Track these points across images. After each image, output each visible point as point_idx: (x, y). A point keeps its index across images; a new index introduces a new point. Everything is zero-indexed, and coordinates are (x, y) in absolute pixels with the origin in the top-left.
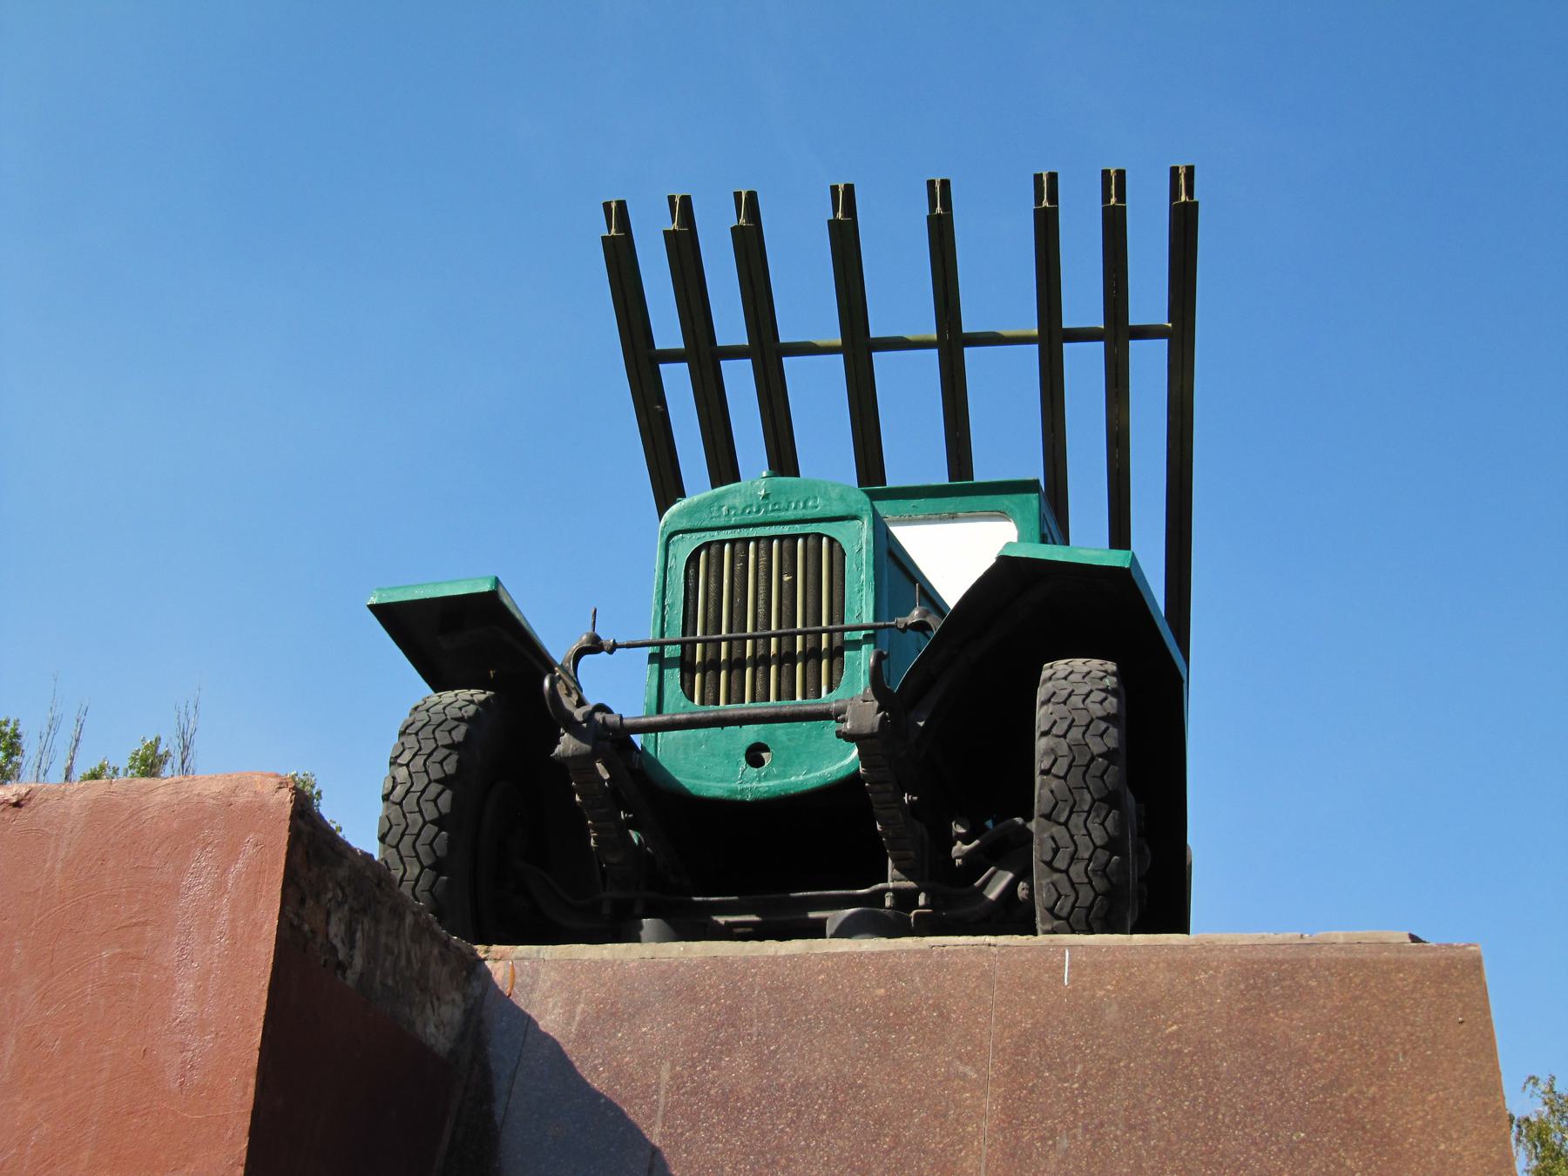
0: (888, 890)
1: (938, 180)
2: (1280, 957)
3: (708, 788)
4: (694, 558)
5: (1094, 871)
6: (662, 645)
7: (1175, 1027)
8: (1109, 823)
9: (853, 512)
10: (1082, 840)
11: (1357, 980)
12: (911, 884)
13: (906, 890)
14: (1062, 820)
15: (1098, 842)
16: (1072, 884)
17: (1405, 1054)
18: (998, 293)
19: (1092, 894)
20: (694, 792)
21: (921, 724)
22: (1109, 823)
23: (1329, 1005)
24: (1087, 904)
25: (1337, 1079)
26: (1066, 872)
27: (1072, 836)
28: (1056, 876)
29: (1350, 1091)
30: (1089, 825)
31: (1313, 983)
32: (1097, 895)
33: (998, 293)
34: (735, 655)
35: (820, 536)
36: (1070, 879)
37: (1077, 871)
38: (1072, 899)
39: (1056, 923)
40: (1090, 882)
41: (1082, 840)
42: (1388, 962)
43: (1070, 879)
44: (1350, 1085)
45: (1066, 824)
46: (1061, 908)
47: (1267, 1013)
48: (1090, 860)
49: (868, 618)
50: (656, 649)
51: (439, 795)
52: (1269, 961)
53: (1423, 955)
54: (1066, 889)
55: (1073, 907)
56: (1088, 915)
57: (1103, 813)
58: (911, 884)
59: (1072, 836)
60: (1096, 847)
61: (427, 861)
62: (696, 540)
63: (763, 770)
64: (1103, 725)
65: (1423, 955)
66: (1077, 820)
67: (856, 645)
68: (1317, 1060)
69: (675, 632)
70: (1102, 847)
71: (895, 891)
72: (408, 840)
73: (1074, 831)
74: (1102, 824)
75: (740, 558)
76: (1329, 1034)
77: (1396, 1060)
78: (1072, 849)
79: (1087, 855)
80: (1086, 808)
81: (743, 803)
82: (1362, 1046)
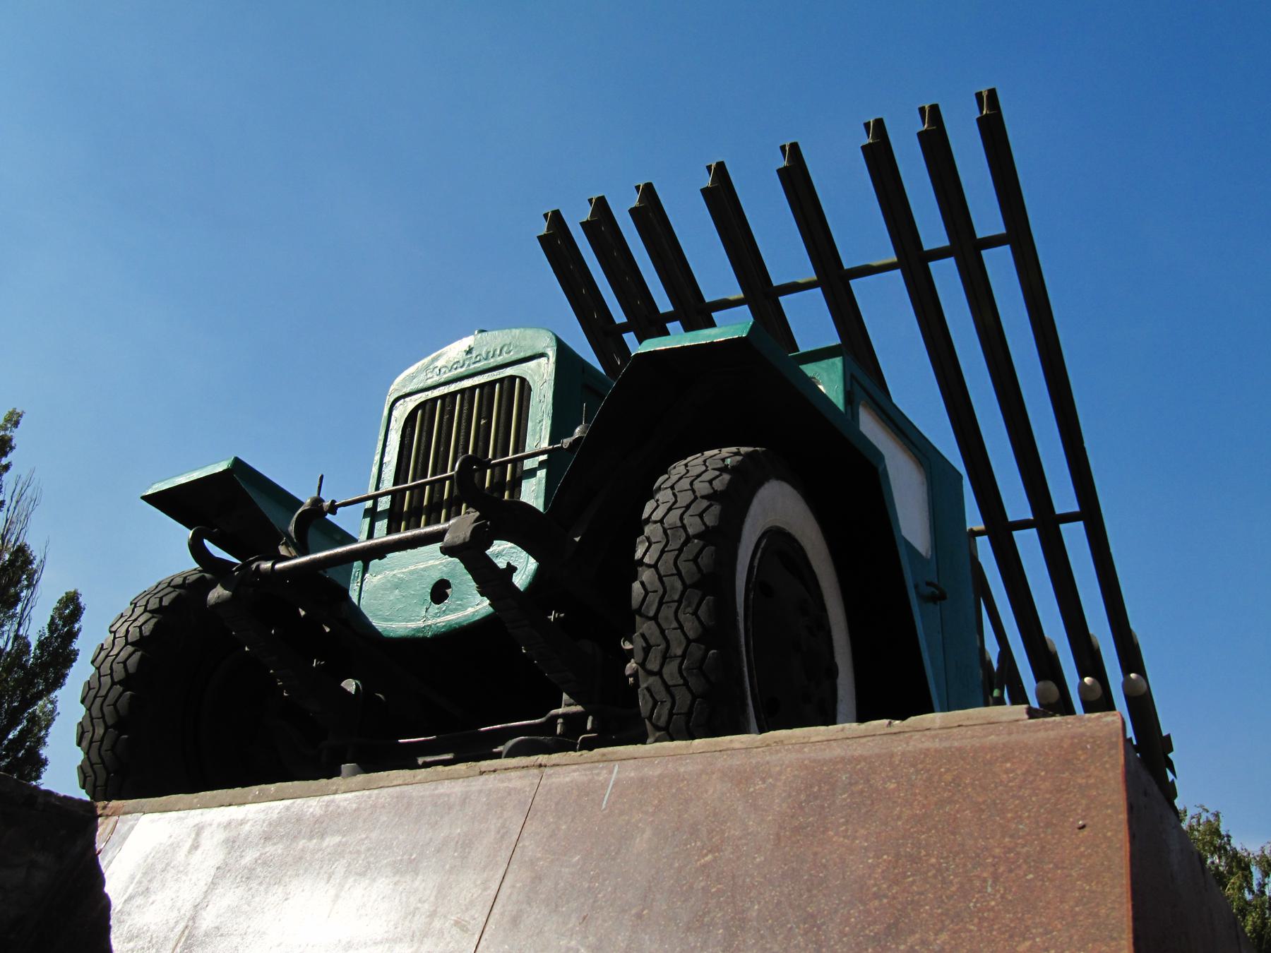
0: (558, 716)
1: (787, 144)
2: (856, 754)
3: (394, 630)
4: (412, 415)
5: (688, 669)
6: (375, 498)
7: (710, 857)
8: (702, 612)
9: (541, 351)
10: (675, 636)
11: (949, 777)
12: (579, 708)
13: (575, 714)
14: (651, 614)
15: (691, 635)
16: (667, 687)
17: (996, 878)
18: (861, 234)
19: (689, 697)
20: (385, 634)
21: (577, 539)
22: (702, 612)
23: (907, 813)
24: (685, 710)
25: (896, 924)
26: (659, 673)
27: (662, 631)
28: (651, 680)
29: (910, 941)
30: (681, 617)
31: (891, 786)
32: (694, 698)
33: (861, 234)
34: (435, 500)
35: (512, 378)
36: (664, 682)
37: (670, 670)
38: (668, 705)
39: (658, 734)
40: (686, 684)
41: (675, 636)
42: (993, 748)
43: (664, 682)
44: (913, 932)
45: (655, 618)
46: (659, 717)
47: (827, 829)
48: (683, 656)
49: (545, 444)
50: (369, 504)
51: (130, 655)
52: (843, 759)
53: (1042, 734)
54: (661, 694)
55: (671, 714)
56: (687, 723)
57: (696, 601)
58: (579, 708)
59: (662, 631)
60: (689, 641)
61: (110, 721)
62: (411, 403)
63: (443, 606)
64: (705, 503)
65: (1042, 734)
66: (668, 612)
67: (532, 473)
68: (876, 896)
69: (388, 484)
70: (695, 641)
71: (564, 716)
72: (99, 700)
73: (664, 626)
74: (695, 613)
75: (448, 412)
76: (898, 856)
77: (982, 890)
78: (663, 646)
79: (679, 652)
80: (676, 597)
81: (424, 639)
82: (939, 870)
